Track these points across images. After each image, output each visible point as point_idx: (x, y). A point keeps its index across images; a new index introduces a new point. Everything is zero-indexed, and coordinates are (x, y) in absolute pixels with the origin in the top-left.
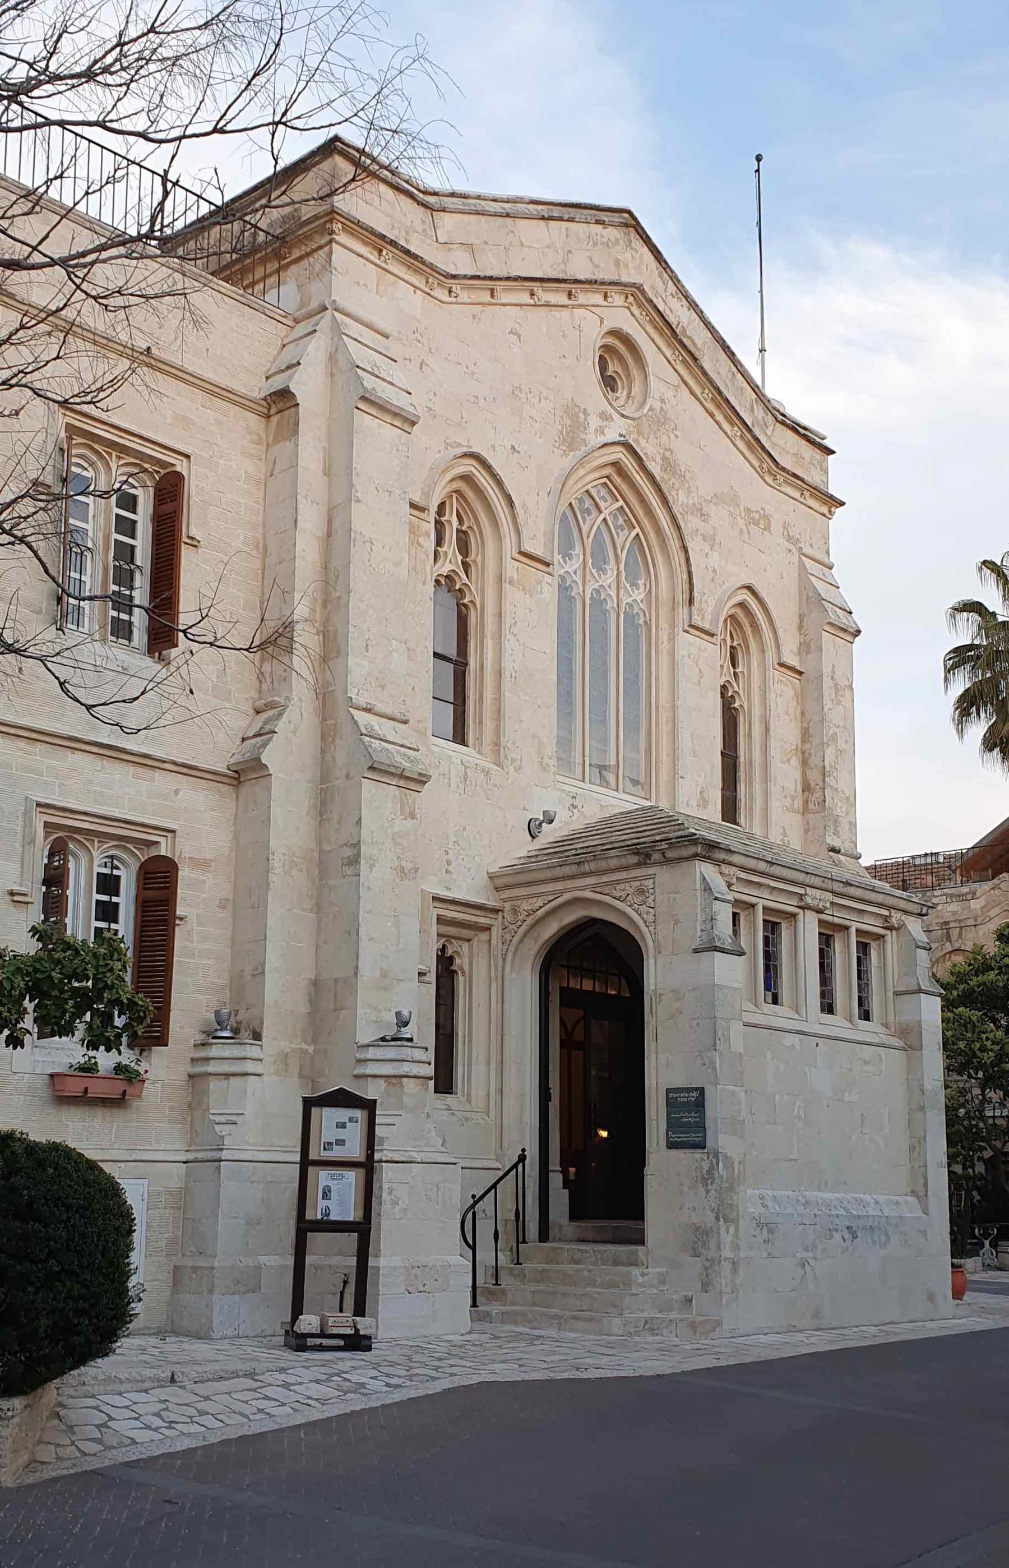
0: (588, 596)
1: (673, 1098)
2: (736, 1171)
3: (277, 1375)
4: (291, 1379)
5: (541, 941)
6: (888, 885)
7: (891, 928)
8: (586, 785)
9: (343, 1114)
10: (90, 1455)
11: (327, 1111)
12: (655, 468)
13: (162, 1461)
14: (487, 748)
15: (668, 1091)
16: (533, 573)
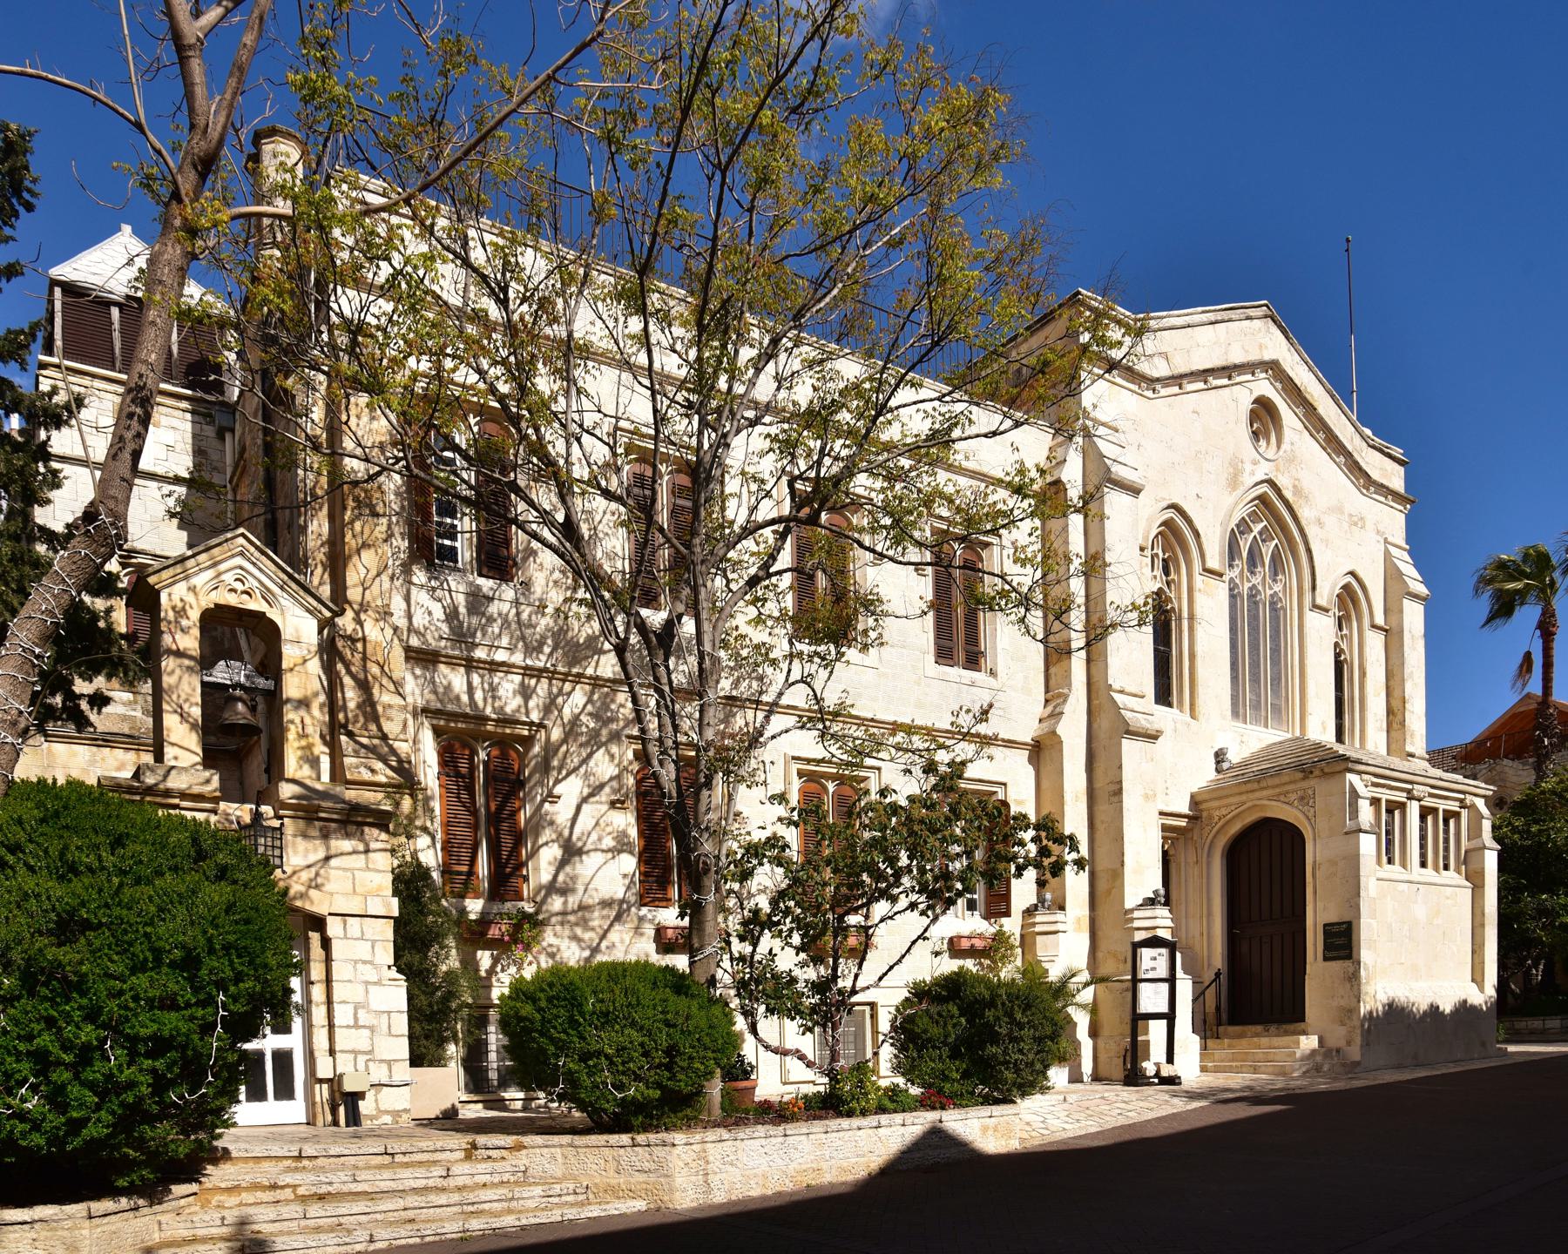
11: (1144, 950)
12: (1288, 494)
15: (1325, 925)
16: (1212, 582)
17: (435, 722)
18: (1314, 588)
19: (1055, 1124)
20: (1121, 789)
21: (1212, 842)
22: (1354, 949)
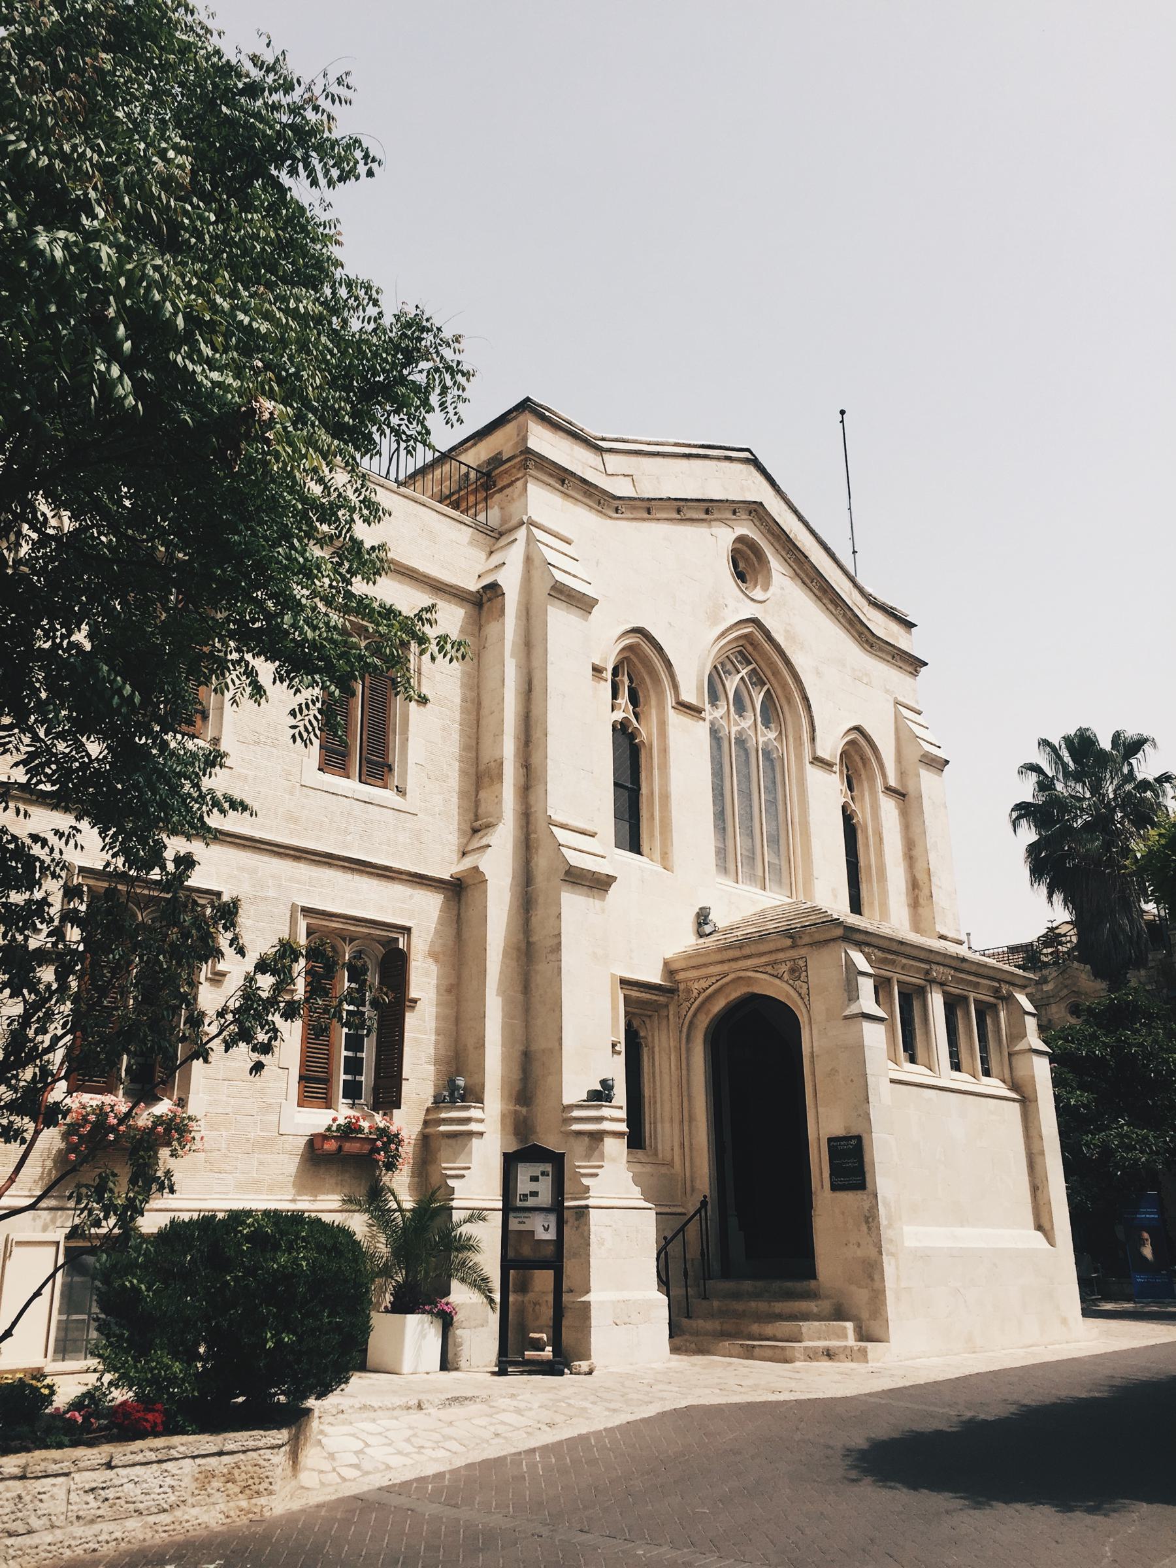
0: (733, 736)
1: (834, 1143)
2: (893, 1210)
3: (508, 1401)
4: (522, 1405)
5: (711, 1016)
6: (995, 961)
7: (1002, 998)
8: (740, 886)
9: (537, 1169)
10: (350, 1480)
13: (415, 1485)
14: (657, 855)
15: (830, 1140)
17: (628, 992)
18: (813, 739)
19: (379, 1453)
20: (560, 944)
21: (691, 1023)
22: (868, 1179)
